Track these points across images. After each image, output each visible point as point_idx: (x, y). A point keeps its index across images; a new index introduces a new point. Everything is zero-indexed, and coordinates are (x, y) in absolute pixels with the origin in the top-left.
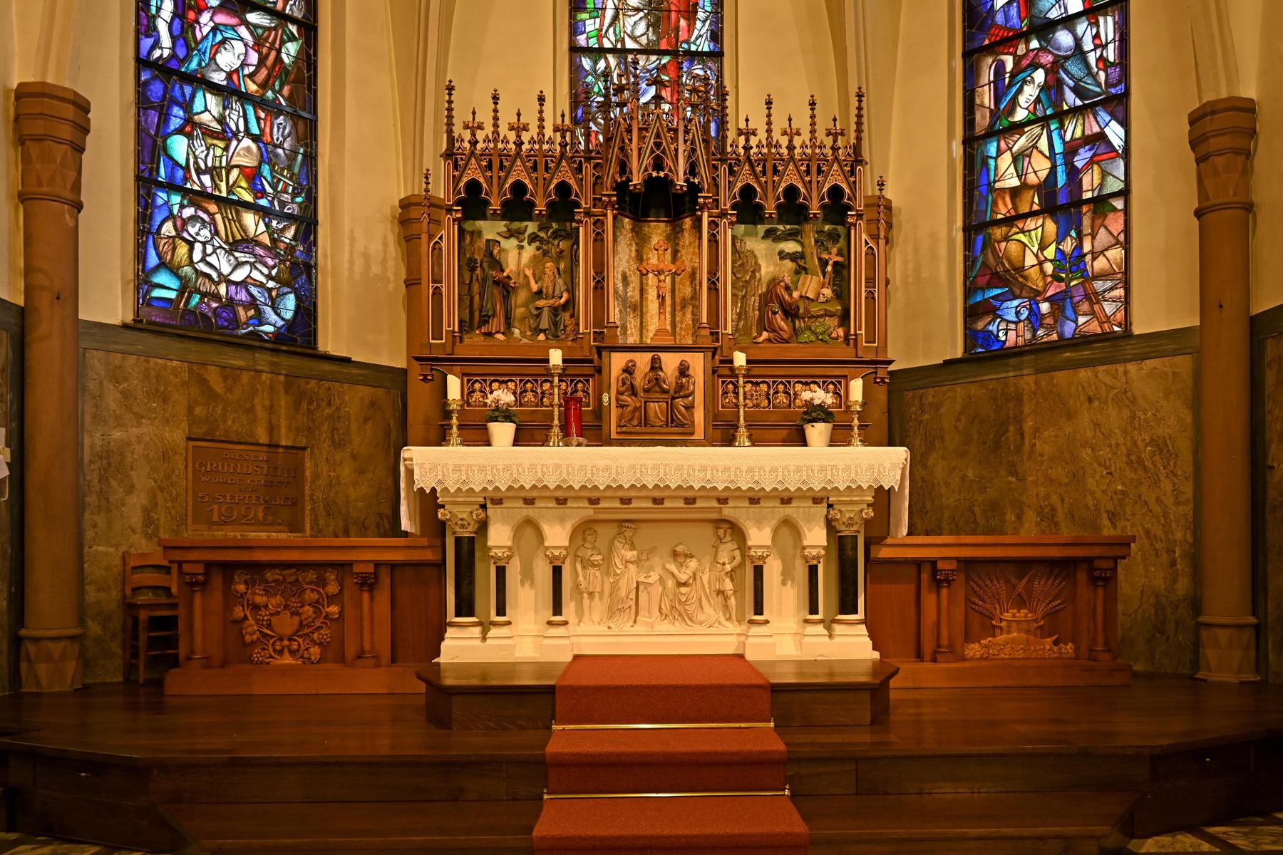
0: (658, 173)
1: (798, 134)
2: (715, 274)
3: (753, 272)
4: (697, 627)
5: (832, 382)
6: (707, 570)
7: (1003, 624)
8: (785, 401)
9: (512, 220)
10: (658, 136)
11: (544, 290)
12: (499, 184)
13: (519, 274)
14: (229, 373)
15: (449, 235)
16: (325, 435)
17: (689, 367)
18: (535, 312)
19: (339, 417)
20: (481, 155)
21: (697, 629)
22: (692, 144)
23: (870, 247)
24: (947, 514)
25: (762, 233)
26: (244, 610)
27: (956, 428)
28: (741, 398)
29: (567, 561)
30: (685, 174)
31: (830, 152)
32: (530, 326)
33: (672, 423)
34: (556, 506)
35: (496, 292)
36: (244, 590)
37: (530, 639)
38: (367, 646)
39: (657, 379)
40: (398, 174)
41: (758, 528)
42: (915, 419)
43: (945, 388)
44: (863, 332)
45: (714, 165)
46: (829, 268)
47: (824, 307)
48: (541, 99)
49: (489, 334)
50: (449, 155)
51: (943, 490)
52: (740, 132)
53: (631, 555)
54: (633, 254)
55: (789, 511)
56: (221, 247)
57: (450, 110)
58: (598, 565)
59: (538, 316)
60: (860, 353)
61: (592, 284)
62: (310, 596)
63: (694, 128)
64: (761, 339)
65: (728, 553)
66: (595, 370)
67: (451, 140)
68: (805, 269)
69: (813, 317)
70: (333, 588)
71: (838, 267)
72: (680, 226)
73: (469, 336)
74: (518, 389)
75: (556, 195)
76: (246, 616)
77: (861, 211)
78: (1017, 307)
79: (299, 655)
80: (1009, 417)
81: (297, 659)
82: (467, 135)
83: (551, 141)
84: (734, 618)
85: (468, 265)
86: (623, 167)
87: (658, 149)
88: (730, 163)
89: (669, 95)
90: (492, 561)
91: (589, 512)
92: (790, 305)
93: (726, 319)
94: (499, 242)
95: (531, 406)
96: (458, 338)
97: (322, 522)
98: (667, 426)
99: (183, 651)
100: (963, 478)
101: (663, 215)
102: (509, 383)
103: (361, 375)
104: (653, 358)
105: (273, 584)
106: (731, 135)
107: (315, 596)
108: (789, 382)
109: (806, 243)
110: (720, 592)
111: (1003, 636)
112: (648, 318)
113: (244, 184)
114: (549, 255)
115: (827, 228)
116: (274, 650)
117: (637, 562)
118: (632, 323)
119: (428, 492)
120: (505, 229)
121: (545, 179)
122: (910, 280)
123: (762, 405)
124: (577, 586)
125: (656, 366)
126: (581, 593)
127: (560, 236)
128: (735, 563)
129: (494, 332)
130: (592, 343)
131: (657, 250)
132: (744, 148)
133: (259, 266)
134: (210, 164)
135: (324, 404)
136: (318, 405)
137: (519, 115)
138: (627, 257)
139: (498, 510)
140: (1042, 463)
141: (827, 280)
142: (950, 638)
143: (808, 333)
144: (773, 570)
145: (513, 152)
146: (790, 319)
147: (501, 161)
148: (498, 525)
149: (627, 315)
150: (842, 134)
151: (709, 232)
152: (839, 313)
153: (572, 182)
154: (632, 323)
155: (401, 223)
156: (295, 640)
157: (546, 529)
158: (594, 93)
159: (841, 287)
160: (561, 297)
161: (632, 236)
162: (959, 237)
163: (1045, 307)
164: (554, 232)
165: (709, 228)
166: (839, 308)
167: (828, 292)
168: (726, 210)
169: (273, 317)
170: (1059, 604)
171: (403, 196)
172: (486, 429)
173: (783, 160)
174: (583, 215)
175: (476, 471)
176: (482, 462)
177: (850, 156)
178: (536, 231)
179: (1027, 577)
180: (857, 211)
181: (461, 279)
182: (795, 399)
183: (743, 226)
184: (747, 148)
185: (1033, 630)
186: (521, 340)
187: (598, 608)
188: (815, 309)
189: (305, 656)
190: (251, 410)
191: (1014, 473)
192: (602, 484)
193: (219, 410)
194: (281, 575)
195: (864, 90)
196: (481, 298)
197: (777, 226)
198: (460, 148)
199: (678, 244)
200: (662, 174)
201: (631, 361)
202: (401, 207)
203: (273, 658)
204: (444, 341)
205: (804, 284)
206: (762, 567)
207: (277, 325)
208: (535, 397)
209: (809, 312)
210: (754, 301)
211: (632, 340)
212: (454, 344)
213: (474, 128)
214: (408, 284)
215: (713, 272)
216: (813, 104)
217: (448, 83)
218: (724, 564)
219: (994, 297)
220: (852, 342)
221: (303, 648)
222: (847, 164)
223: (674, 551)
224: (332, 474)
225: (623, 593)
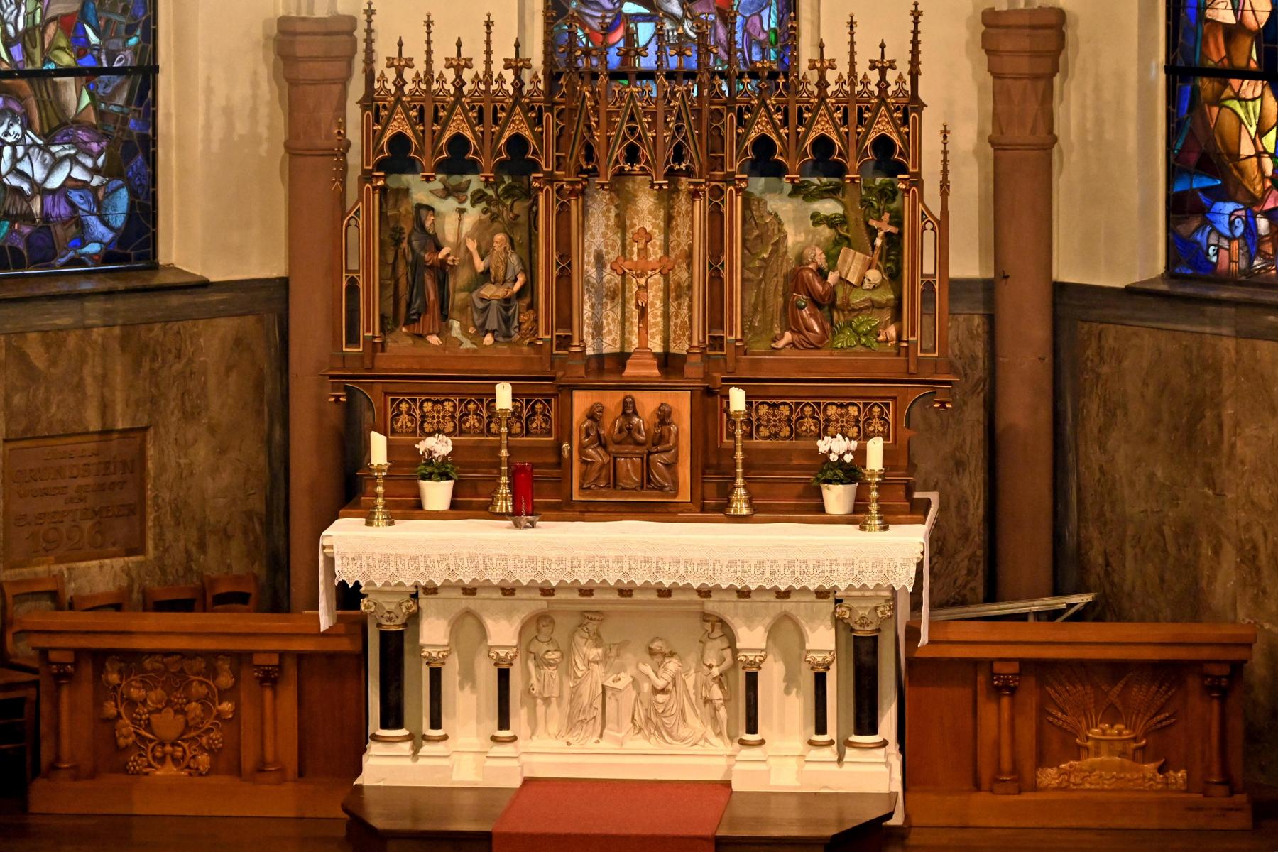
0: (632, 166)
2: (719, 258)
4: (678, 744)
6: (692, 671)
7: (1089, 744)
8: (813, 428)
10: (632, 118)
11: (492, 272)
12: (433, 140)
14: (54, 339)
15: (368, 210)
16: (173, 404)
18: (480, 305)
19: (192, 373)
21: (678, 747)
24: (1131, 530)
26: (117, 706)
27: (1143, 396)
29: (517, 662)
34: (502, 597)
36: (118, 681)
37: (471, 757)
38: (269, 756)
41: (749, 627)
43: (1129, 329)
46: (878, 242)
47: (868, 295)
51: (1126, 492)
53: (594, 653)
54: (612, 222)
55: (787, 605)
56: (34, 144)
58: (556, 665)
61: (555, 272)
62: (198, 689)
65: (714, 653)
69: (854, 310)
70: (225, 680)
74: (458, 412)
76: (119, 713)
78: (1231, 215)
79: (184, 764)
80: (1205, 395)
81: (182, 770)
82: (391, 74)
84: (725, 733)
85: (392, 237)
90: (425, 661)
91: (541, 604)
96: (379, 347)
97: (169, 536)
98: (642, 487)
99: (46, 755)
100: (1151, 478)
102: (446, 404)
103: (222, 302)
104: (625, 404)
105: (152, 674)
107: (203, 690)
108: (818, 405)
110: (707, 701)
111: (1089, 760)
113: (63, 43)
115: (879, 180)
116: (154, 758)
117: (605, 661)
118: (611, 316)
119: (350, 586)
123: (782, 434)
124: (528, 690)
125: (629, 410)
126: (535, 698)
128: (725, 665)
130: (555, 352)
133: (82, 158)
134: (20, 26)
135: (171, 357)
136: (164, 361)
138: (603, 229)
139: (432, 601)
140: (1244, 473)
142: (1014, 762)
144: (772, 677)
148: (432, 619)
149: (602, 308)
154: (611, 316)
156: (179, 745)
157: (490, 624)
160: (516, 280)
161: (611, 199)
162: (1160, 79)
163: (1263, 224)
164: (506, 190)
167: (874, 275)
169: (99, 229)
170: (1167, 719)
172: (418, 488)
175: (406, 562)
176: (413, 551)
178: (482, 187)
179: (1123, 682)
183: (763, 179)
185: (1131, 752)
186: (462, 343)
187: (555, 716)
188: (857, 299)
189: (192, 765)
190: (80, 386)
191: (1211, 483)
192: (555, 579)
193: (41, 393)
194: (163, 663)
197: (809, 179)
199: (672, 207)
203: (153, 767)
204: (361, 349)
206: (756, 674)
207: (105, 241)
208: (480, 422)
209: (848, 304)
210: (776, 284)
218: (710, 667)
219: (1205, 190)
221: (189, 755)
223: (650, 649)
224: (182, 461)
225: (585, 700)
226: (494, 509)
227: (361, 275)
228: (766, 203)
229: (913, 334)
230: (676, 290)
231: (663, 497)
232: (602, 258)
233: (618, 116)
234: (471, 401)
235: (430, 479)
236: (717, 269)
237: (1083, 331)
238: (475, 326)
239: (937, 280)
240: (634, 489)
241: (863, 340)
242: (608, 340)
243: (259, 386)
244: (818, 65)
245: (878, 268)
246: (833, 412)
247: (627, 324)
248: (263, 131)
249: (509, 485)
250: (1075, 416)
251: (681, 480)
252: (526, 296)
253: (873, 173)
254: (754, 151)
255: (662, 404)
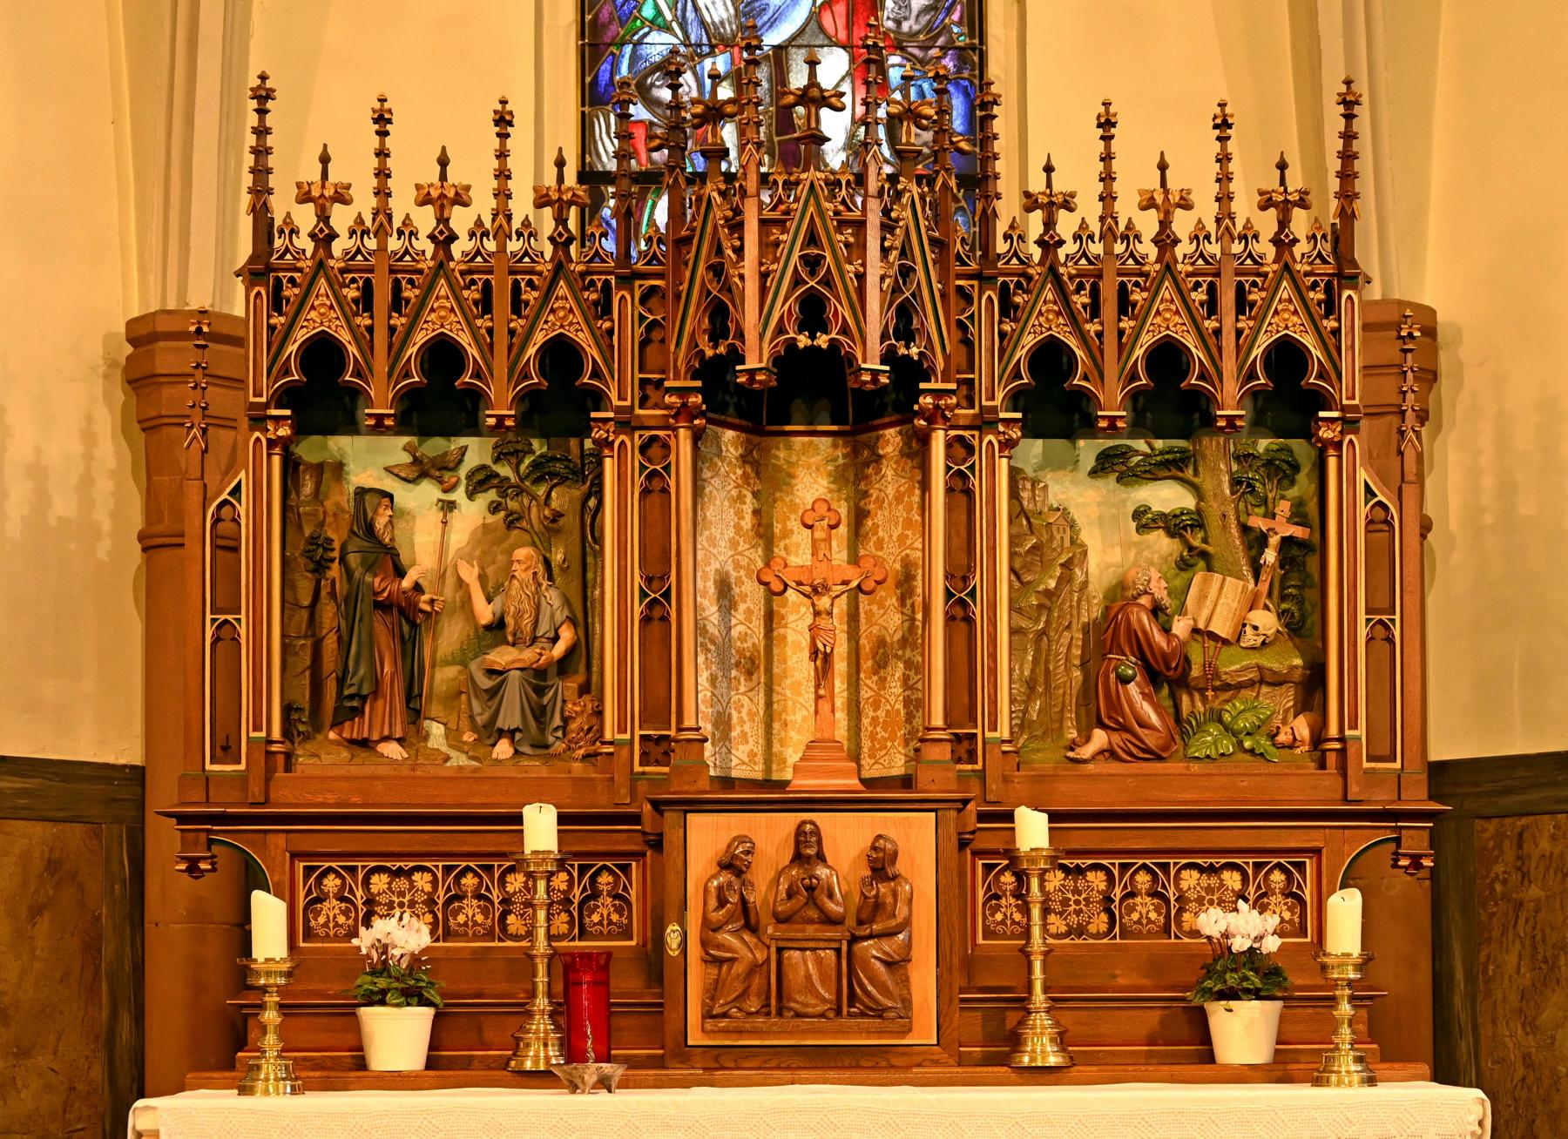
0: (813, 337)
1: (1186, 205)
2: (965, 579)
3: (1067, 566)
5: (1279, 866)
8: (1153, 916)
9: (425, 432)
10: (812, 239)
11: (510, 621)
12: (390, 347)
13: (442, 576)
17: (895, 854)
18: (486, 683)
20: (343, 271)
22: (903, 254)
23: (1380, 503)
25: (1089, 461)
28: (1036, 912)
30: (884, 337)
31: (1270, 252)
32: (471, 717)
33: (850, 1005)
35: (381, 627)
39: (811, 889)
40: (124, 246)
42: (1504, 896)
44: (1361, 732)
45: (960, 289)
46: (1270, 556)
47: (1255, 659)
48: (503, 121)
49: (365, 744)
50: (260, 271)
52: (1030, 202)
54: (748, 522)
57: (261, 152)
59: (494, 692)
60: (1354, 791)
61: (638, 610)
63: (908, 213)
64: (1087, 751)
66: (647, 842)
67: (264, 228)
68: (1204, 555)
69: (1226, 687)
71: (1295, 552)
72: (873, 449)
73: (308, 746)
74: (441, 892)
75: (542, 372)
77: (1355, 408)
82: (305, 218)
83: (528, 231)
86: (720, 318)
87: (812, 274)
88: (1005, 284)
89: (841, 22)
92: (1166, 658)
93: (994, 702)
94: (391, 497)
95: (476, 937)
96: (281, 760)
98: (838, 1012)
101: (825, 415)
102: (417, 876)
104: (799, 831)
106: (1008, 208)
109: (1208, 485)
112: (785, 690)
114: (524, 524)
115: (1263, 444)
118: (746, 705)
120: (407, 458)
121: (512, 332)
122: (1488, 519)
123: (1092, 929)
125: (807, 850)
127: (553, 475)
129: (375, 737)
130: (637, 768)
131: (810, 527)
132: (1040, 242)
137: (443, 162)
138: (731, 533)
141: (1264, 587)
143: (1214, 729)
145: (427, 264)
146: (1165, 691)
147: (397, 283)
149: (729, 688)
150: (1303, 204)
151: (948, 468)
152: (1297, 675)
153: (583, 338)
154: (746, 705)
155: (129, 382)
158: (644, 20)
159: (1300, 602)
160: (555, 640)
161: (745, 476)
164: (535, 465)
165: (948, 456)
166: (1298, 662)
167: (1266, 621)
168: (994, 410)
171: (136, 314)
172: (356, 1027)
173: (1146, 275)
174: (611, 426)
177: (1325, 261)
178: (489, 462)
180: (1343, 409)
181: (289, 597)
182: (1181, 911)
183: (1040, 442)
184: (1049, 244)
186: (447, 758)
188: (1232, 665)
195: (1361, 87)
196: (344, 644)
197: (1128, 442)
198: (287, 250)
199: (866, 495)
200: (822, 341)
201: (742, 839)
202: (131, 340)
204: (242, 767)
205: (1203, 597)
208: (485, 912)
209: (1217, 675)
210: (1069, 644)
211: (743, 761)
212: (269, 772)
213: (325, 197)
214: (151, 544)
215: (959, 575)
216: (1223, 124)
217: (257, 82)
220: (1332, 759)
222: (1315, 285)
226: (522, 1063)
227: (243, 616)
228: (1046, 487)
229: (1354, 726)
230: (874, 655)
231: (880, 1033)
232: (730, 588)
233: (785, 231)
234: (468, 869)
235: (382, 1003)
236: (961, 602)
237: (1487, 835)
238: (474, 728)
239: (1397, 617)
240: (822, 1015)
241: (1247, 744)
242: (740, 752)
243: (92, 947)
244: (1159, 199)
245: (1266, 607)
246: (1193, 882)
247: (776, 725)
248: (102, 517)
249: (552, 1015)
250: (1471, 979)
251: (917, 999)
252: (576, 672)
253: (1251, 434)
254: (1032, 369)
255: (879, 837)
